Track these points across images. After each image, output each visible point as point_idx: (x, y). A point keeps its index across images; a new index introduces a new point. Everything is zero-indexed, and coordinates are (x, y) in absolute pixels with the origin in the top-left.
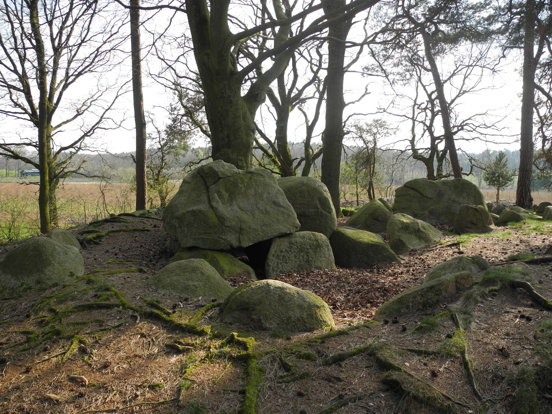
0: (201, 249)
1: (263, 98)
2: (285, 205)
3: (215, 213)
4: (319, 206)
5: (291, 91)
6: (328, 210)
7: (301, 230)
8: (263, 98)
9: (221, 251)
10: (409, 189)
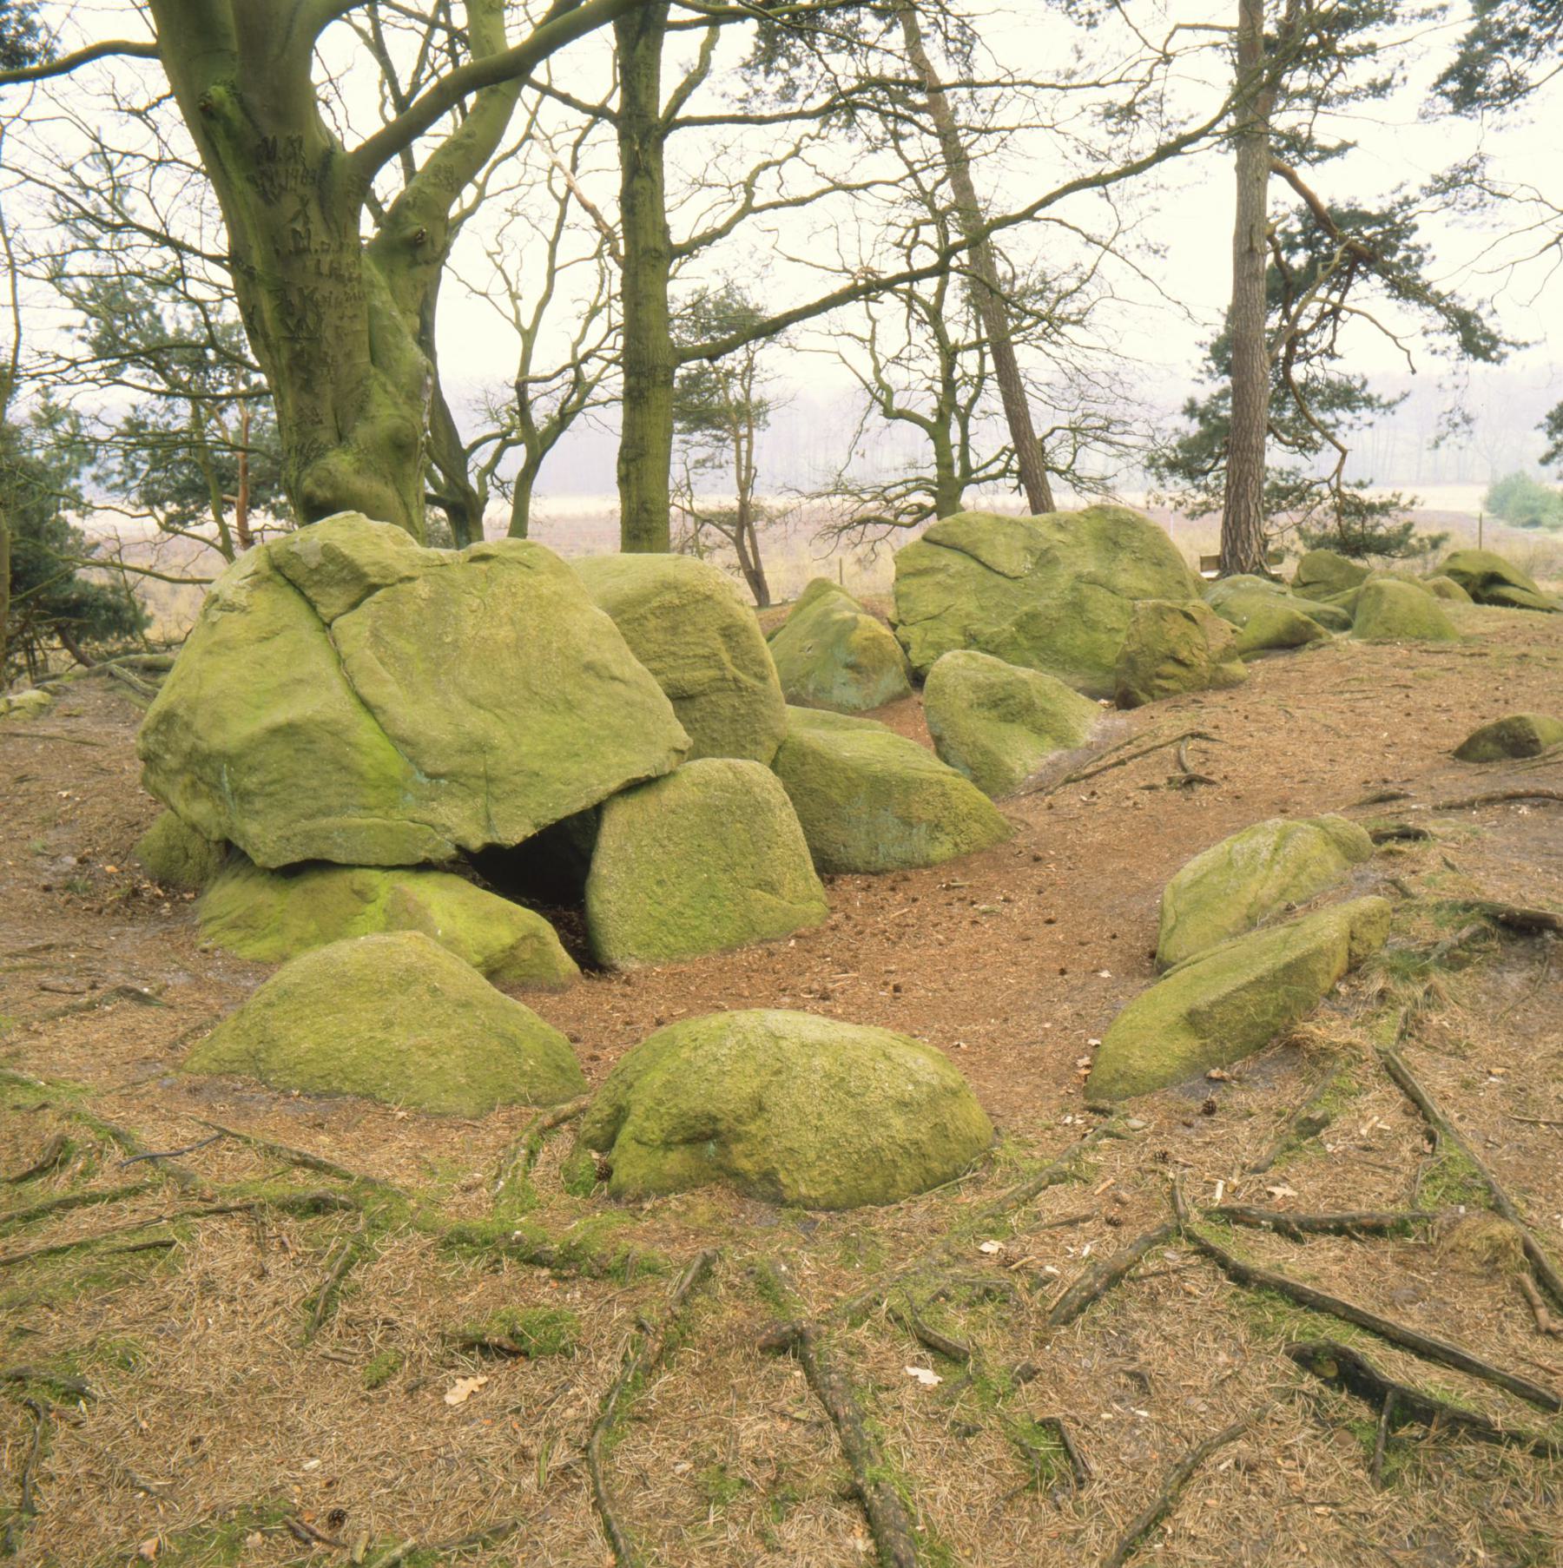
0: (1061, 1224)
1: (438, 249)
2: (627, 673)
3: (381, 726)
4: (726, 657)
5: (416, 86)
6: (942, 850)
7: (696, 754)
8: (438, 249)
9: (424, 867)
10: (942, 549)
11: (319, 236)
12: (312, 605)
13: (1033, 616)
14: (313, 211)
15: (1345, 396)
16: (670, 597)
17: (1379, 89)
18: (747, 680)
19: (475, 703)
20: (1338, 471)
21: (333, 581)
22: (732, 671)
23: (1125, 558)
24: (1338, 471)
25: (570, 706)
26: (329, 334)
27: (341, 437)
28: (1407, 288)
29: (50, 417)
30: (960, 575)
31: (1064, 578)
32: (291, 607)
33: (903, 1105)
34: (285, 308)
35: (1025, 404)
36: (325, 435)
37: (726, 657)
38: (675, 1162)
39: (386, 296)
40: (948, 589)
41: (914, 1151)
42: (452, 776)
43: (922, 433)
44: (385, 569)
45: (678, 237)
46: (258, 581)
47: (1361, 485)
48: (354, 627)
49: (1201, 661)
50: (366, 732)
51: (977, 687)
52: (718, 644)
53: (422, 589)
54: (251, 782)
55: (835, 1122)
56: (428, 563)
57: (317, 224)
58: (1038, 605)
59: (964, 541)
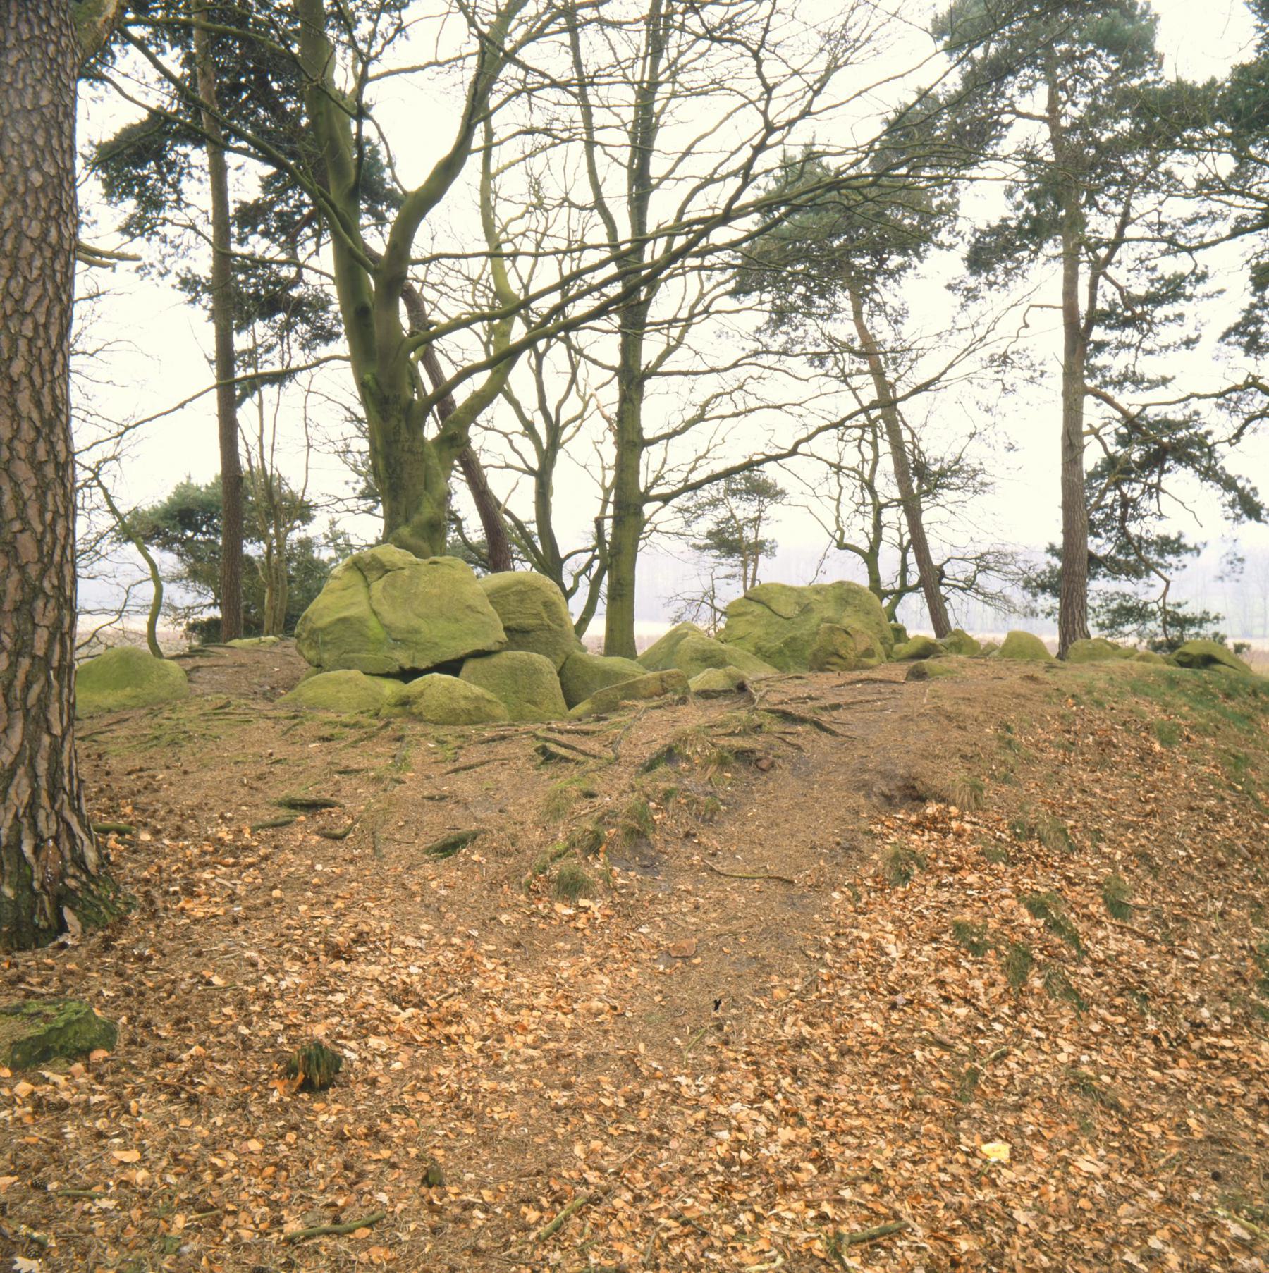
4: (544, 615)
9: (387, 675)
11: (405, 434)
12: (365, 578)
13: (793, 639)
14: (403, 425)
15: (1172, 546)
16: (521, 587)
17: (1189, 343)
18: (554, 626)
19: (418, 616)
20: (1164, 596)
21: (373, 568)
22: (547, 621)
23: (850, 610)
24: (1164, 596)
25: (457, 621)
26: (406, 476)
27: (407, 521)
28: (1210, 474)
29: (334, 537)
30: (759, 616)
31: (815, 618)
32: (356, 578)
33: (466, 698)
34: (388, 465)
35: (925, 541)
36: (400, 520)
37: (544, 615)
38: (396, 710)
39: (436, 461)
40: (751, 623)
41: (468, 713)
42: (403, 641)
43: (859, 558)
44: (394, 564)
45: (647, 434)
46: (347, 568)
47: (1179, 605)
48: (377, 586)
49: (851, 656)
50: (373, 622)
51: (696, 651)
52: (541, 608)
53: (406, 572)
54: (328, 638)
55: (443, 699)
56: (411, 563)
57: (403, 430)
58: (798, 634)
59: (764, 598)
